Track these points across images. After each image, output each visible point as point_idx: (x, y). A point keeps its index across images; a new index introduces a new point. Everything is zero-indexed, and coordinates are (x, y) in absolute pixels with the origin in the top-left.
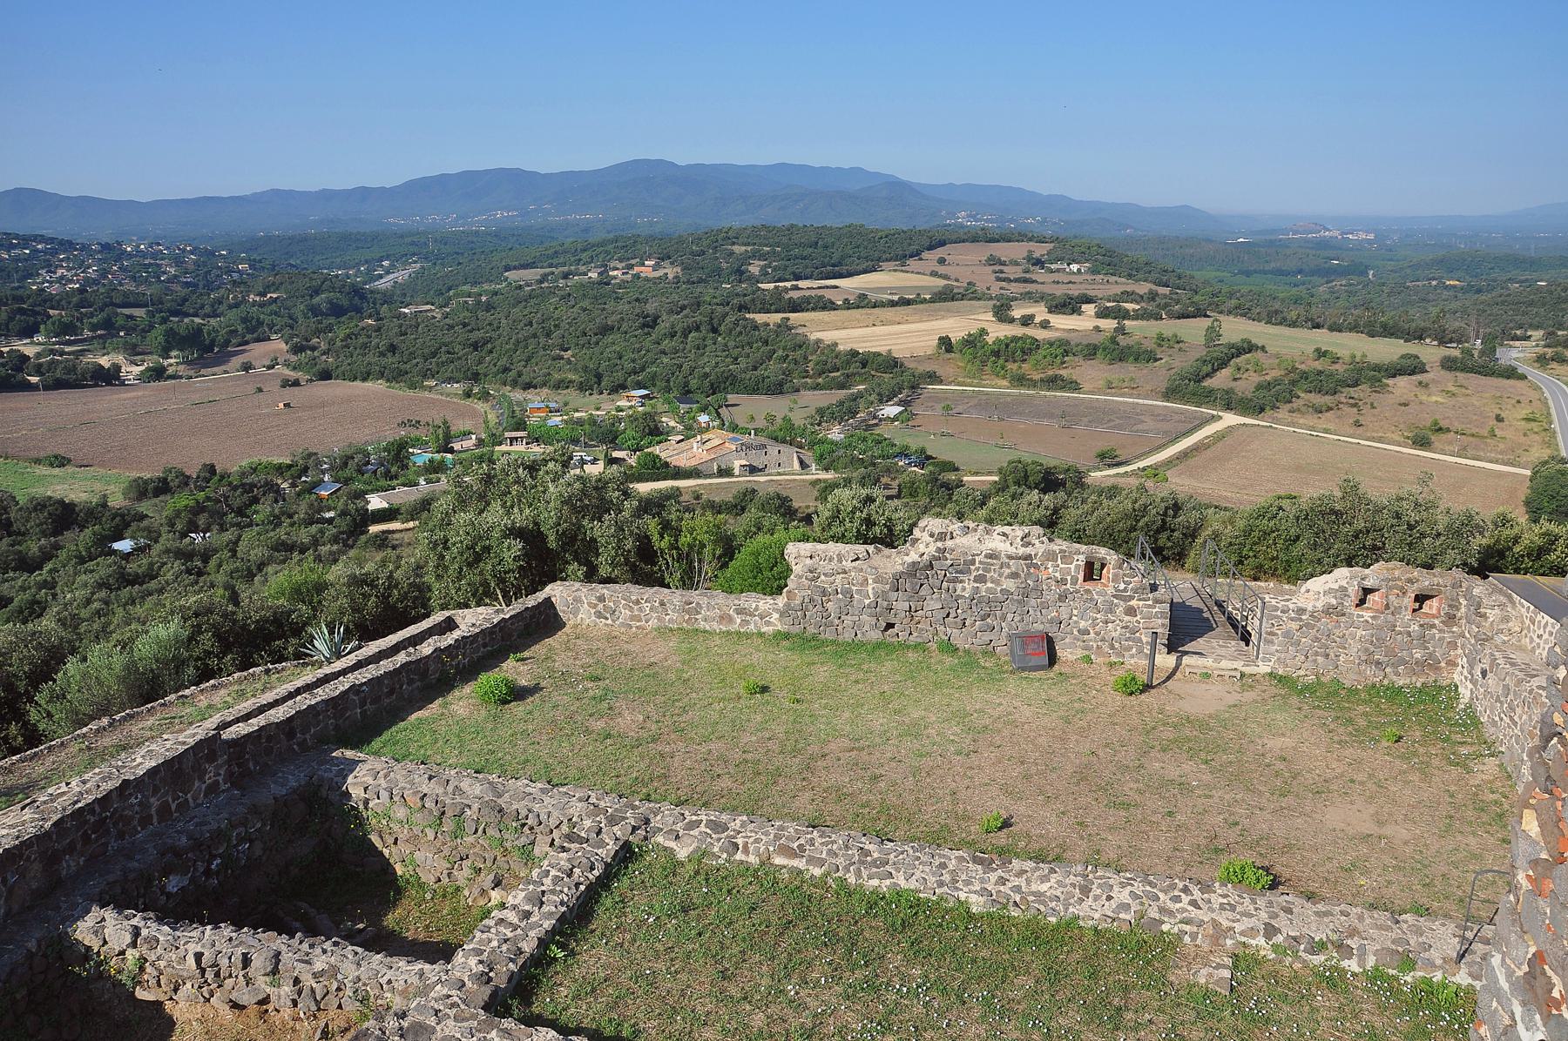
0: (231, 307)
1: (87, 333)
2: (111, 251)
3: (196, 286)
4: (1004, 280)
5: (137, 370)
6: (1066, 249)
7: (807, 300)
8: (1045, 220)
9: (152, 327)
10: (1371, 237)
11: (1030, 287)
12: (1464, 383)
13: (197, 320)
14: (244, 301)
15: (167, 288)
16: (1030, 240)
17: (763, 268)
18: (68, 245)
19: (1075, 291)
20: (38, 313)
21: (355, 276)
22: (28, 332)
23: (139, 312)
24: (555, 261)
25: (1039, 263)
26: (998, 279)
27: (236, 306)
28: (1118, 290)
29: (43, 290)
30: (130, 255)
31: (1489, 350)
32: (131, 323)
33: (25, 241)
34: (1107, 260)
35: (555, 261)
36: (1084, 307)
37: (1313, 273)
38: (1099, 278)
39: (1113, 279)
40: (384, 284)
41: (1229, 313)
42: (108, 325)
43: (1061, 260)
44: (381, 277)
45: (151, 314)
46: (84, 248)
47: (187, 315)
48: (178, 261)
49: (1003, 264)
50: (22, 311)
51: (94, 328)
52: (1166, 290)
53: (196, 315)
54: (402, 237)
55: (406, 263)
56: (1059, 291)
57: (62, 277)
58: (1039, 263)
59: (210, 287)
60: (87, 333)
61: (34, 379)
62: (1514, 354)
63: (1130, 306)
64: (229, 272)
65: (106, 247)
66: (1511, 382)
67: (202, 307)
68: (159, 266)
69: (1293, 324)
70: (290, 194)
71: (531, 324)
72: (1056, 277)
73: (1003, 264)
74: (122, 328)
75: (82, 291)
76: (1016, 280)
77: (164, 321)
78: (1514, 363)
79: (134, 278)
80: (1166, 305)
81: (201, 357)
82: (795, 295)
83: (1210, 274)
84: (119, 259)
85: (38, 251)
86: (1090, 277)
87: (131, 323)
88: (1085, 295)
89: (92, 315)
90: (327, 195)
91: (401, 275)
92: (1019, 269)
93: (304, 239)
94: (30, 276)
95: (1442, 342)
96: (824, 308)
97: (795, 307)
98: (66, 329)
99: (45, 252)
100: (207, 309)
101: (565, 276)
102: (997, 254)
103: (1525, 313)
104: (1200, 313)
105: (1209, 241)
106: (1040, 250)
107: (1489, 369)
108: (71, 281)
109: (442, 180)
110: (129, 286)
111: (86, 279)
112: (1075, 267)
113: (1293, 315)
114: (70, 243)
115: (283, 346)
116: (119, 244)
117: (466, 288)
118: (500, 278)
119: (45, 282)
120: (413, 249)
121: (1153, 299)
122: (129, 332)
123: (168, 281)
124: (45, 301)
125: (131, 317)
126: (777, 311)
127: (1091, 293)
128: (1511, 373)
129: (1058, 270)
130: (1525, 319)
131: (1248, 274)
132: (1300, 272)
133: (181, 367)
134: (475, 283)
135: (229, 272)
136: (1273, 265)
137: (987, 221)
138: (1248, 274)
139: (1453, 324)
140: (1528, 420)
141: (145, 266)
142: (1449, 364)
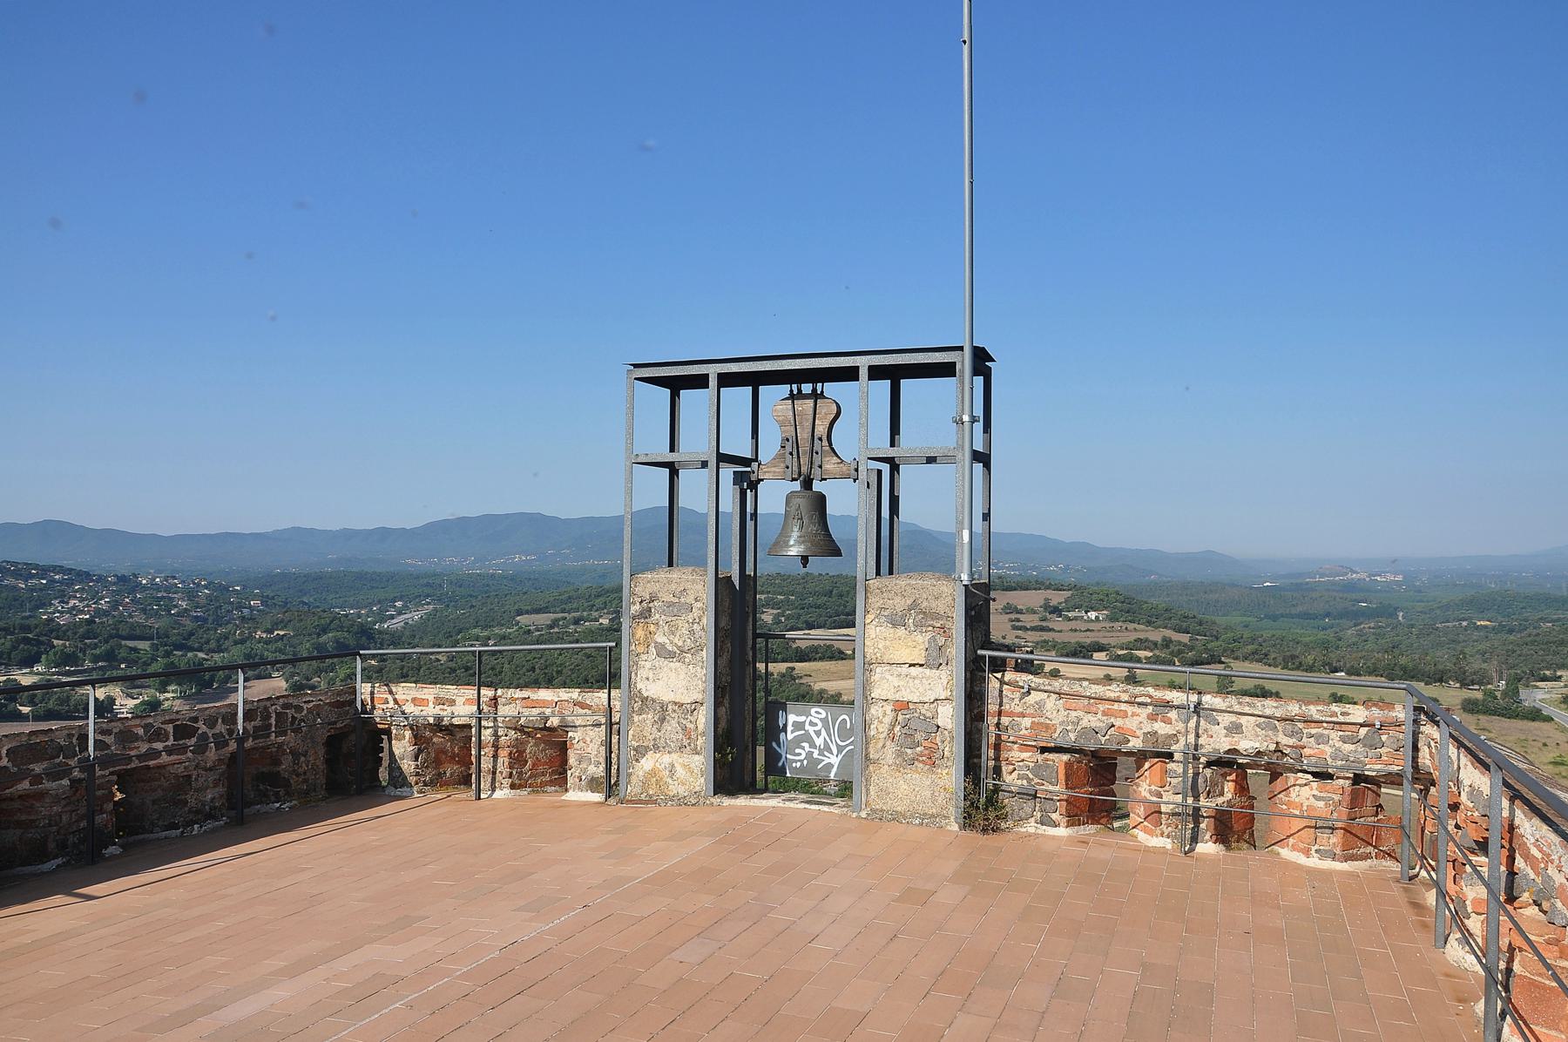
0: (236, 643)
1: (88, 664)
2: (127, 583)
3: (205, 620)
4: (1020, 628)
5: (131, 703)
6: (1084, 596)
7: (815, 649)
8: (1067, 567)
9: (154, 659)
10: (1400, 578)
11: (1046, 636)
12: (1487, 725)
13: (201, 655)
14: (250, 637)
15: (176, 622)
16: (1048, 588)
17: (776, 617)
18: (84, 576)
19: (1088, 639)
20: (40, 643)
21: (365, 615)
22: (28, 662)
23: (144, 645)
24: (567, 607)
25: (1056, 611)
26: (1015, 628)
27: (242, 642)
28: (1133, 637)
29: (52, 620)
30: (145, 588)
31: (1512, 692)
32: (134, 656)
33: (44, 571)
34: (1125, 606)
35: (567, 607)
36: (1096, 655)
37: (1341, 616)
38: (1117, 625)
39: (1131, 626)
40: (397, 623)
41: (1245, 658)
42: (110, 657)
43: (1079, 607)
44: (392, 617)
45: (155, 648)
46: (101, 579)
47: (192, 649)
48: (191, 595)
49: (1020, 612)
50: (27, 641)
51: (96, 659)
52: (1185, 638)
53: (200, 650)
54: (417, 578)
55: (419, 604)
56: (1074, 639)
57: (74, 608)
58: (1056, 611)
59: (219, 622)
60: (88, 664)
61: (25, 710)
62: (1540, 695)
63: (1142, 654)
64: (240, 607)
65: (122, 579)
66: (1536, 724)
67: (207, 642)
68: (171, 599)
69: (1310, 669)
70: (311, 532)
71: (533, 669)
72: (1073, 625)
73: (1020, 612)
74: (124, 660)
75: (90, 622)
76: (1033, 629)
77: (168, 654)
78: (1538, 705)
79: (144, 611)
80: (1180, 652)
81: (198, 692)
82: (803, 645)
83: (1235, 619)
84: (133, 591)
85: (55, 581)
86: (1108, 625)
87: (134, 656)
88: (1097, 643)
89: (96, 646)
90: (348, 535)
91: (415, 616)
92: (1036, 617)
93: (319, 577)
94: (43, 605)
95: (1464, 685)
96: (831, 658)
97: (803, 656)
98: (67, 659)
99: (61, 582)
100: (213, 645)
101: (577, 622)
102: (1013, 602)
103: (1556, 653)
104: (1214, 660)
105: (1233, 585)
106: (1057, 598)
107: (1512, 710)
108: (82, 612)
109: (463, 522)
110: (139, 618)
111: (97, 611)
112: (1092, 615)
113: (1310, 659)
114: (87, 574)
115: (284, 684)
116: (135, 576)
117: (476, 631)
118: (511, 622)
119: (58, 613)
120: (427, 590)
121: (1167, 646)
122: (130, 663)
123: (178, 614)
124: (51, 631)
125: (135, 650)
126: (783, 661)
127: (1104, 641)
128: (1535, 715)
129: (1076, 618)
130: (1557, 659)
131: (1274, 618)
132: (1328, 615)
133: (177, 702)
134: (485, 627)
135: (240, 607)
136: (1299, 609)
137: (1009, 568)
138: (1274, 618)
139: (1476, 664)
140: (1555, 763)
141: (159, 598)
142: (1470, 707)
